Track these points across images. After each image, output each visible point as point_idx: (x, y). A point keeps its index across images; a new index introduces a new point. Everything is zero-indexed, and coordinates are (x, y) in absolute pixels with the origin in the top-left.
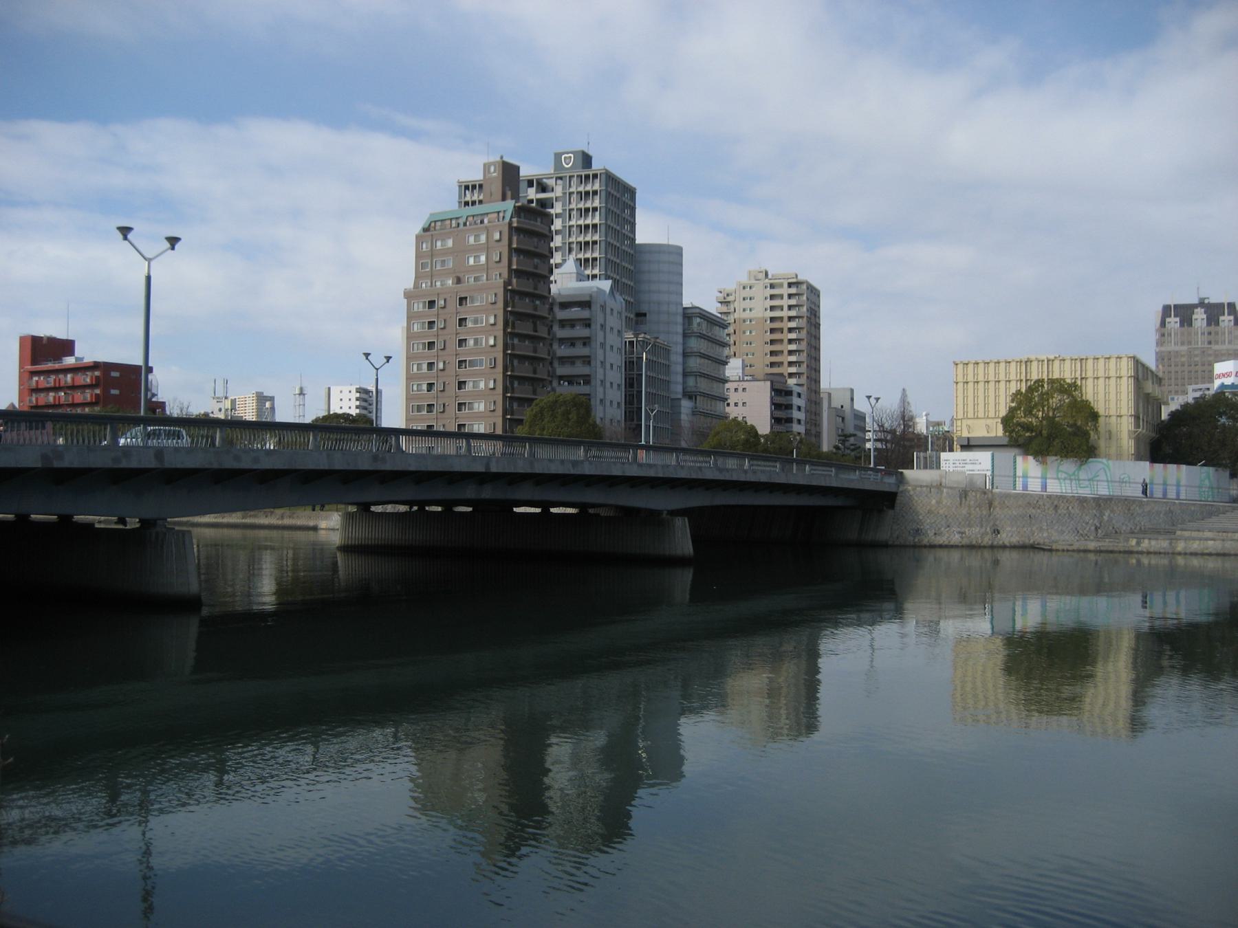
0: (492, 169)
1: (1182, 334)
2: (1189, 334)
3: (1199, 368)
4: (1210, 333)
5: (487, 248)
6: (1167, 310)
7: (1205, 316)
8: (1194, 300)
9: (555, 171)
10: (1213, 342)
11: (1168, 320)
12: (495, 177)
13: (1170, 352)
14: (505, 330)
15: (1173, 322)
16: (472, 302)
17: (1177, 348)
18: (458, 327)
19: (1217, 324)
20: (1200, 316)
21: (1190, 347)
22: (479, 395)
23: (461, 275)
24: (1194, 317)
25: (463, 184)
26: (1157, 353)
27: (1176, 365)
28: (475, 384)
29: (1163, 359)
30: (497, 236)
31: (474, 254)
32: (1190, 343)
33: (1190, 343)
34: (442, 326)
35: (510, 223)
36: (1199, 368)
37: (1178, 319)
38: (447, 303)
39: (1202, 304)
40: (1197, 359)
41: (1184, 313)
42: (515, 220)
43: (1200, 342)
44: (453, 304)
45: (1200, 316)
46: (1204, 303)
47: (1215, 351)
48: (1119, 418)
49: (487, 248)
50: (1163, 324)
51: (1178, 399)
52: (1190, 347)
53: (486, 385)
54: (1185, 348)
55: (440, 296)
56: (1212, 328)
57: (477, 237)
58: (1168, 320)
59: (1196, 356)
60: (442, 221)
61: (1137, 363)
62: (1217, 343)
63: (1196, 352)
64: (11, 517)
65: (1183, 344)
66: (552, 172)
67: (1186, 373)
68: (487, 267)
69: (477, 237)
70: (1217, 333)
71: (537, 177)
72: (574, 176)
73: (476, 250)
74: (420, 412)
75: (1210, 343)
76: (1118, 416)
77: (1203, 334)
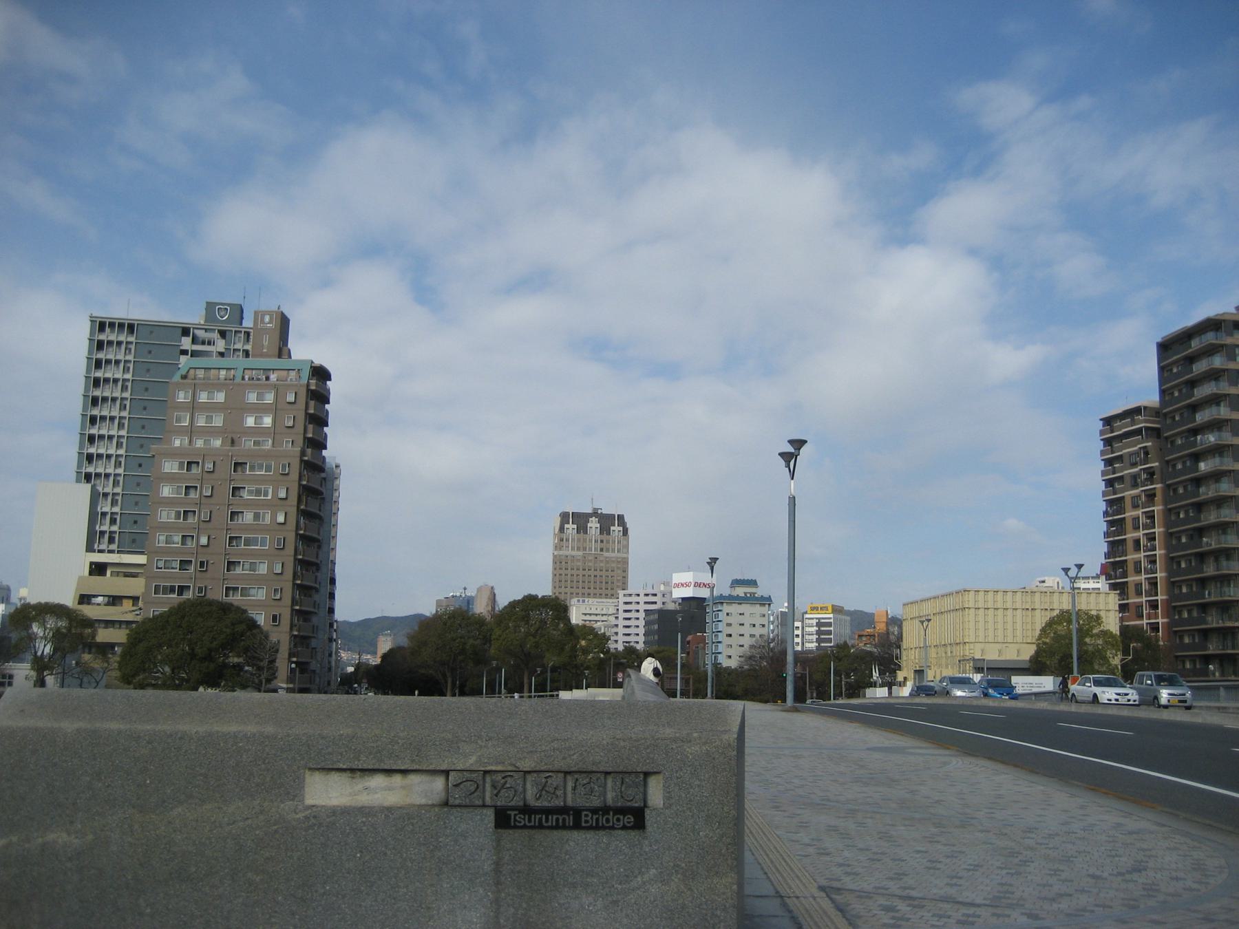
0: (267, 319)
1: (579, 540)
2: (585, 540)
3: (604, 573)
4: (602, 541)
5: (275, 409)
6: (565, 517)
7: (598, 525)
8: (588, 510)
9: (206, 321)
10: (604, 550)
11: (566, 526)
12: (270, 329)
13: (567, 556)
14: (298, 507)
15: (571, 527)
16: (252, 468)
17: (575, 553)
18: (231, 497)
19: (609, 533)
20: (594, 524)
21: (585, 552)
22: (260, 581)
23: (236, 437)
24: (589, 525)
25: (98, 320)
26: (555, 556)
27: (572, 569)
28: (253, 567)
29: (561, 563)
30: (291, 398)
31: (207, 414)
32: (585, 549)
33: (585, 549)
34: (209, 494)
35: (308, 385)
36: (581, 572)
37: (575, 526)
38: (216, 468)
39: (595, 513)
40: (590, 564)
41: (581, 520)
42: (313, 382)
43: (593, 548)
44: (225, 470)
45: (594, 524)
46: (597, 513)
47: (606, 558)
48: (1014, 611)
49: (275, 409)
50: (562, 529)
51: (588, 601)
52: (585, 552)
53: (270, 568)
54: (581, 553)
55: (206, 457)
56: (605, 537)
57: (260, 396)
58: (566, 526)
59: (590, 561)
60: (227, 369)
61: (708, 563)
62: (608, 550)
63: (590, 558)
64: (565, 695)
65: (578, 549)
66: (202, 322)
67: (569, 575)
68: (273, 432)
69: (260, 396)
70: (608, 542)
71: (101, 320)
72: (241, 332)
73: (259, 410)
74: (182, 595)
75: (602, 550)
76: (985, 608)
77: (573, 540)
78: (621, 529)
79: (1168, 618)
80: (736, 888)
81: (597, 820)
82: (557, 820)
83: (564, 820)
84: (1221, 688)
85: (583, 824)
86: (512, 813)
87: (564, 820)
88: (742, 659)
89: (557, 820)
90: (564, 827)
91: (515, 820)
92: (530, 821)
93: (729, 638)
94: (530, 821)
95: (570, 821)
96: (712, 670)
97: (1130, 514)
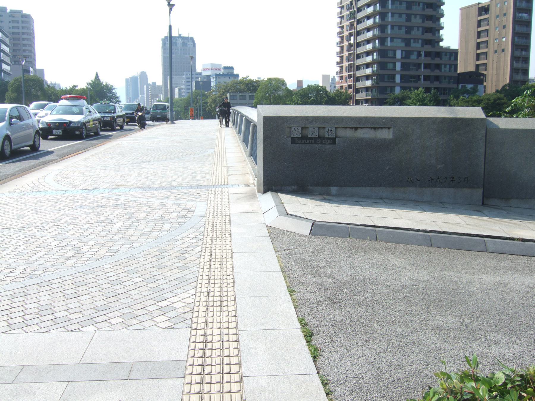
4: (184, 50)
75: (184, 54)
77: (181, 50)
78: (192, 43)
79: (240, 81)
80: (335, 188)
81: (321, 141)
82: (309, 141)
83: (311, 141)
84: (520, 71)
85: (317, 142)
86: (296, 139)
87: (311, 141)
88: (32, 125)
89: (309, 141)
90: (311, 144)
91: (297, 141)
92: (301, 141)
93: (259, 77)
94: (301, 141)
95: (313, 141)
96: (71, 122)
97: (345, 13)
